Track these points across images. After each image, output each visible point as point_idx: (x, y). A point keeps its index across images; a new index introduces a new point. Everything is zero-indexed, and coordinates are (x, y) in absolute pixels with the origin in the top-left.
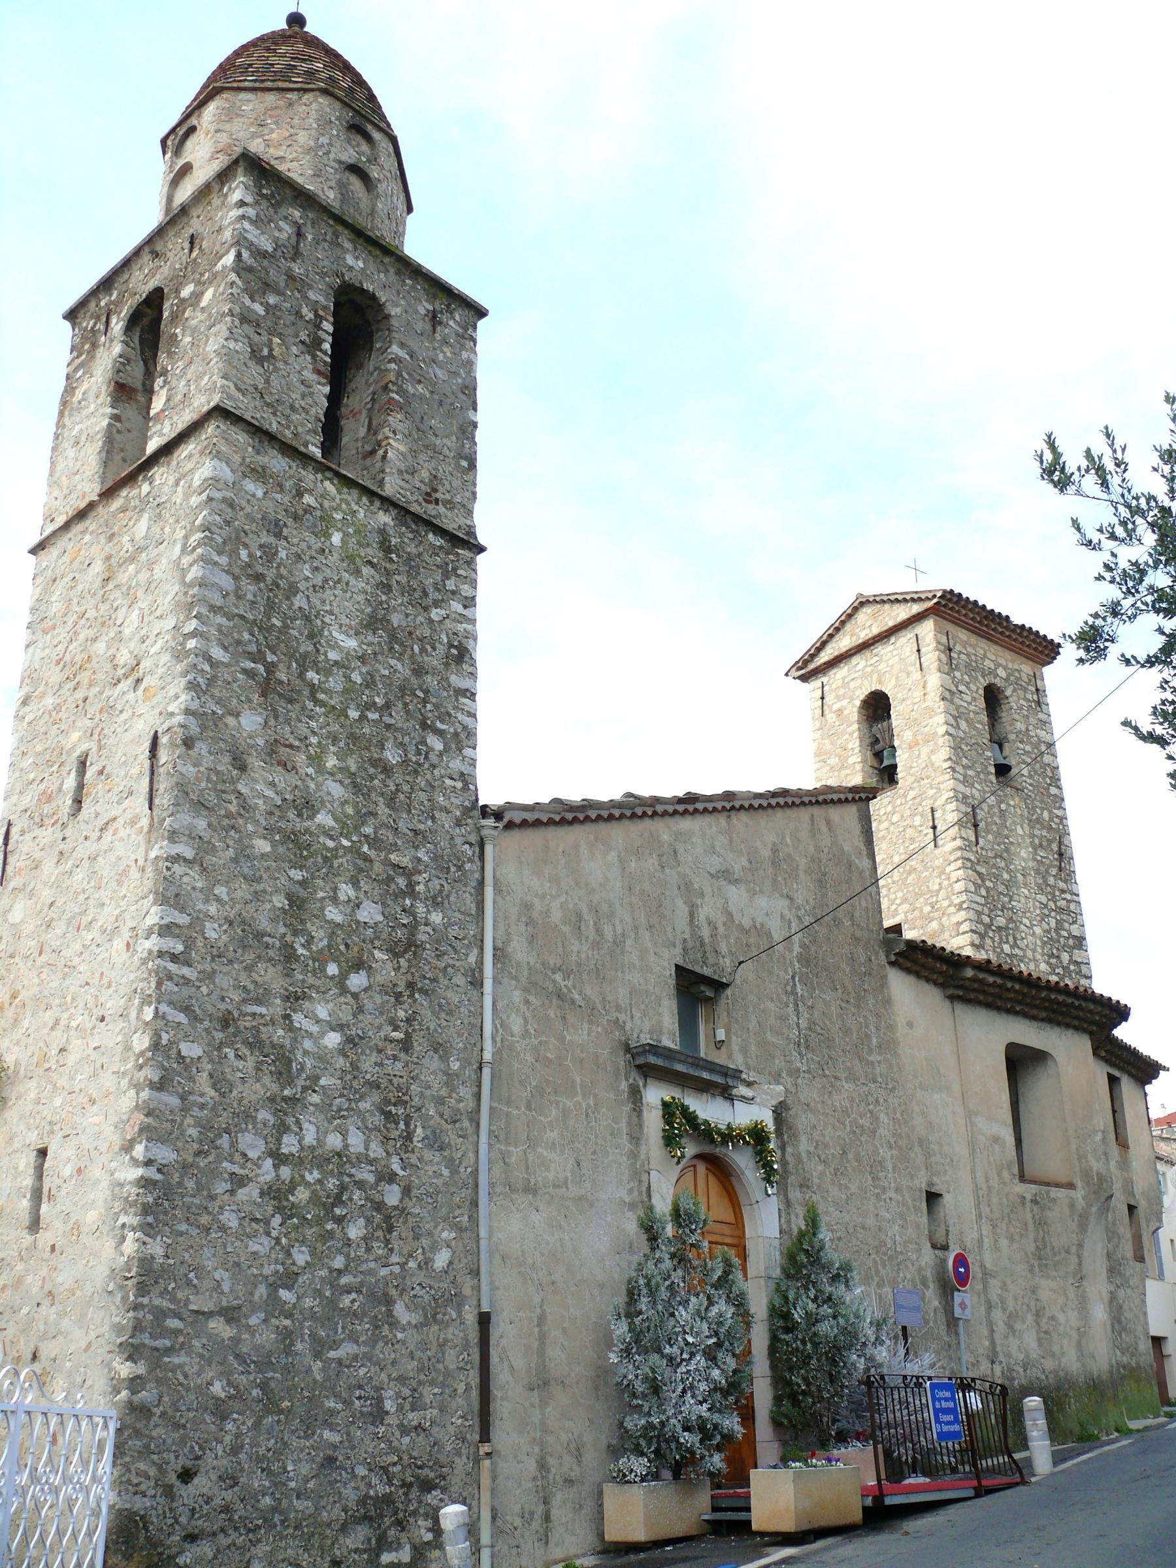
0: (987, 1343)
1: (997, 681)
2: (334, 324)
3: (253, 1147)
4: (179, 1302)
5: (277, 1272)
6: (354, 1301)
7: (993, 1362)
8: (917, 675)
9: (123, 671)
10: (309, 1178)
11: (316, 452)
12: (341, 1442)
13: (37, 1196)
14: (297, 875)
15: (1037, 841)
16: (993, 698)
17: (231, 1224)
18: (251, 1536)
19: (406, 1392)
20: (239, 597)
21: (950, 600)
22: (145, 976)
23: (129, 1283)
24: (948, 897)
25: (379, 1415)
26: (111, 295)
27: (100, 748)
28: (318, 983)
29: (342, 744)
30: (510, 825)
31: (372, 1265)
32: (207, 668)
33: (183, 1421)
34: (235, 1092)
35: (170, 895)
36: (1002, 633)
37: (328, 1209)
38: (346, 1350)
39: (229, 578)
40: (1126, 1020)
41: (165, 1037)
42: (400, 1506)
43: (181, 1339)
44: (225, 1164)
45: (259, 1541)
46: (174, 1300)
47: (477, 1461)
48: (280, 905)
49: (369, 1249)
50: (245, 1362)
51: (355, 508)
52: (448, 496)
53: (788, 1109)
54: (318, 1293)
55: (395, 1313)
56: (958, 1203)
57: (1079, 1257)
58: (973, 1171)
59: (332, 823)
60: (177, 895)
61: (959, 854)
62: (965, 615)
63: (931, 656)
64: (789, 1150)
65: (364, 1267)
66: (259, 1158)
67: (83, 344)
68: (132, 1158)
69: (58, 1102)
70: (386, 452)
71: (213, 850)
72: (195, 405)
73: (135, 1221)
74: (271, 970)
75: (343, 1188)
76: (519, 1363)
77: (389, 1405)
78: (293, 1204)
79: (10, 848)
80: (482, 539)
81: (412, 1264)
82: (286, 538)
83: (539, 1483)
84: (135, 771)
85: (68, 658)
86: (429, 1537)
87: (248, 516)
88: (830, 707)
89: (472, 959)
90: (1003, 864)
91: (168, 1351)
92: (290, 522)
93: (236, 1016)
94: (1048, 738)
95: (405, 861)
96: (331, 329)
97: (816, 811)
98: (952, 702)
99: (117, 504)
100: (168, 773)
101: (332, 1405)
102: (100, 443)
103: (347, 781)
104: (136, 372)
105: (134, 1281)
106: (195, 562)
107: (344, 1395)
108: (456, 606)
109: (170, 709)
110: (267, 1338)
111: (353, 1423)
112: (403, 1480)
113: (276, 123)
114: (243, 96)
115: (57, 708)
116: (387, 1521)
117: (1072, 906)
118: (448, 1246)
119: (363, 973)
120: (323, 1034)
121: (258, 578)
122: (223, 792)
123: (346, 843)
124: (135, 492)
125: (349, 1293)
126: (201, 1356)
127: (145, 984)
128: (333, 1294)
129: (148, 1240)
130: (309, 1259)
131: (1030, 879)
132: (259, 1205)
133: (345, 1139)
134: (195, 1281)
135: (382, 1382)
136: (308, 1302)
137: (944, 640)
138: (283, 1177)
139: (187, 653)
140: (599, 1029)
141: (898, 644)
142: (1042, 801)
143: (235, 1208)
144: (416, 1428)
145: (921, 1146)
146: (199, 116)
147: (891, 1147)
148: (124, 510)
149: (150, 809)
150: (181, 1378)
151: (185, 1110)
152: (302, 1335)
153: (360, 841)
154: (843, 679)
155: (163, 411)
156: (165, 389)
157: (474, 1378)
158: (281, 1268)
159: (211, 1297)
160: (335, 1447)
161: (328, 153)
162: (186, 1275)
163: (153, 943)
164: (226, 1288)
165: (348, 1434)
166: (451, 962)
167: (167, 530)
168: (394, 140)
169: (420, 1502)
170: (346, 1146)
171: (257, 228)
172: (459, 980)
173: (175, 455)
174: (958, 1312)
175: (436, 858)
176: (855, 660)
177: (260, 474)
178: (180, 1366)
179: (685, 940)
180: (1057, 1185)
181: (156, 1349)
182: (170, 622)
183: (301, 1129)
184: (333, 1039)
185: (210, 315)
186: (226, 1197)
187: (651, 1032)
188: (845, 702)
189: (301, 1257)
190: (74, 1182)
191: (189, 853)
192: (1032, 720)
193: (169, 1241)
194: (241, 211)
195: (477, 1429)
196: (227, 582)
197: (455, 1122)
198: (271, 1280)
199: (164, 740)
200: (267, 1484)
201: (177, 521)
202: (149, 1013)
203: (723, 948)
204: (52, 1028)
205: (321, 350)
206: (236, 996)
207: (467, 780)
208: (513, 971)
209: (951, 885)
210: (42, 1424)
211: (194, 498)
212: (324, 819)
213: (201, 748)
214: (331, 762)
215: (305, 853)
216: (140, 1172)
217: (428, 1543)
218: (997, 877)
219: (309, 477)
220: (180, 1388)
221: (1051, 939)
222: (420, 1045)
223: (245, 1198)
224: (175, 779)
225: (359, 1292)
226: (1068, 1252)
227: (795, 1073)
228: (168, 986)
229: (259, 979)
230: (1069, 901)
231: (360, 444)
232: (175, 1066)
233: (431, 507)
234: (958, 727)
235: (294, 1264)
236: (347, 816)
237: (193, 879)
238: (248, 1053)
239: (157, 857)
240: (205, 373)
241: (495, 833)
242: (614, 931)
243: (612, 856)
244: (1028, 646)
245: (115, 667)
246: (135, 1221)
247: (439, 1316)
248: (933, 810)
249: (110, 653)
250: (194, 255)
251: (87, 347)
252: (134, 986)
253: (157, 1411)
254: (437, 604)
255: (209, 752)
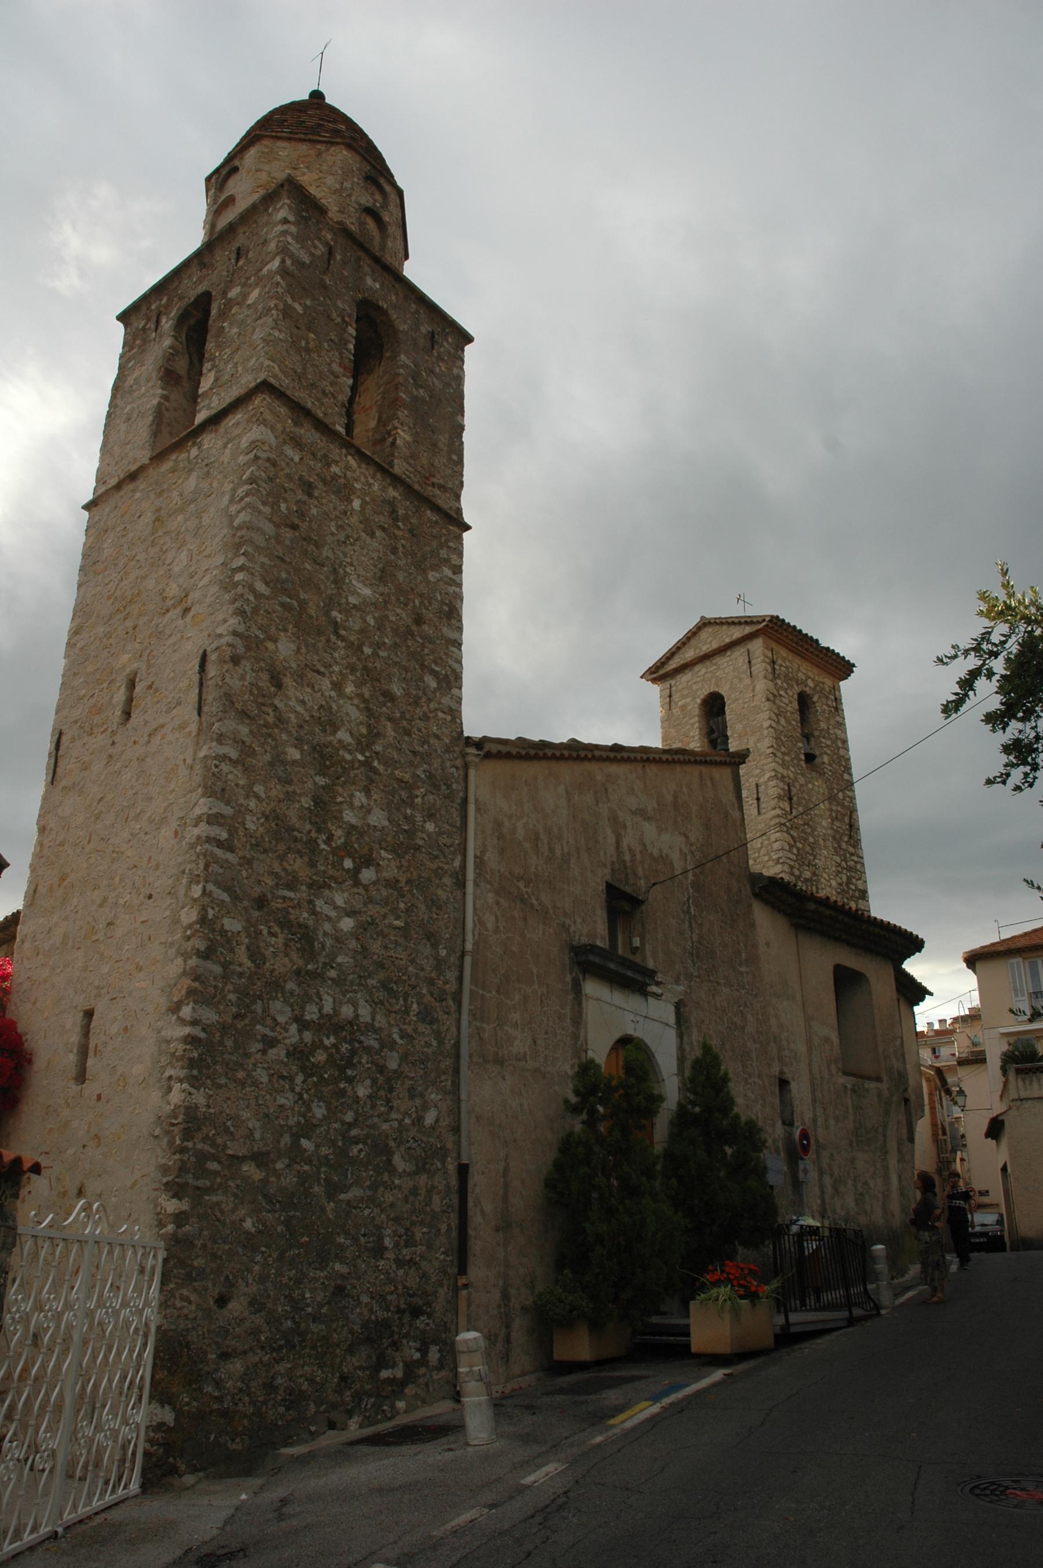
0: (819, 1201)
1: (807, 689)
2: (357, 330)
3: (282, 1013)
4: (218, 1146)
5: (299, 1123)
6: (360, 1151)
7: (823, 1217)
8: (748, 681)
9: (172, 602)
10: (327, 1042)
11: (340, 429)
12: (349, 1273)
13: (84, 1052)
14: (321, 781)
15: (834, 814)
16: (804, 702)
17: (262, 1080)
18: (275, 1354)
19: (402, 1231)
20: (279, 542)
21: (776, 624)
22: (193, 858)
23: (176, 1129)
24: (768, 854)
25: (379, 1251)
26: (161, 300)
27: (149, 667)
28: (337, 874)
29: (358, 674)
30: (488, 756)
31: (376, 1120)
32: (252, 598)
33: (219, 1253)
34: (268, 964)
35: (215, 788)
36: (812, 653)
37: (342, 1070)
38: (355, 1193)
39: (271, 525)
40: (920, 951)
41: (211, 913)
42: (396, 1329)
43: (219, 1180)
44: (258, 1027)
45: (282, 1359)
46: (214, 1144)
47: (456, 1290)
48: (307, 806)
49: (373, 1107)
50: (272, 1202)
51: (371, 481)
52: (441, 482)
53: (685, 1006)
54: (333, 1143)
55: (393, 1162)
56: (800, 1090)
57: (884, 1135)
58: (810, 1064)
59: (349, 740)
60: (223, 790)
61: (777, 820)
62: (786, 637)
63: (760, 666)
64: (685, 1039)
65: (369, 1122)
66: (286, 1023)
67: (134, 340)
68: (179, 1018)
69: (105, 969)
70: (395, 440)
71: (253, 753)
72: (243, 382)
73: (183, 1073)
74: (299, 861)
75: (353, 1052)
76: (488, 1207)
77: (387, 1242)
78: (313, 1064)
79: (61, 753)
80: (467, 518)
81: (407, 1121)
82: (317, 498)
83: (502, 1310)
84: (184, 684)
85: (118, 593)
86: (417, 1356)
87: (287, 475)
88: (676, 703)
89: (457, 864)
90: (809, 831)
91: (208, 1190)
92: (320, 485)
93: (270, 897)
94: (842, 736)
95: (407, 777)
96: (354, 333)
97: (704, 769)
98: (774, 702)
99: (167, 466)
100: (217, 685)
101: (342, 1240)
102: (151, 418)
103: (362, 706)
104: (181, 365)
105: (182, 1126)
106: (243, 509)
107: (353, 1232)
108: (448, 572)
109: (219, 631)
110: (289, 1181)
111: (359, 1257)
112: (398, 1307)
113: (307, 167)
114: (280, 144)
115: (108, 635)
116: (386, 1342)
117: (859, 866)
118: (436, 1106)
119: (372, 868)
120: (339, 918)
121: (294, 527)
122: (263, 705)
123: (360, 757)
124: (184, 456)
125: (357, 1143)
126: (236, 1195)
127: (194, 865)
128: (344, 1144)
129: (192, 1090)
130: (325, 1112)
131: (829, 843)
132: (286, 1065)
133: (356, 1010)
134: (232, 1129)
135: (382, 1222)
136: (324, 1151)
137: (769, 654)
138: (306, 1041)
139: (236, 585)
140: (551, 931)
141: (733, 656)
142: (838, 784)
143: (265, 1065)
144: (409, 1261)
145: (775, 1041)
146: (242, 158)
147: (755, 1042)
148: (174, 470)
149: (199, 715)
150: (218, 1214)
151: (225, 977)
152: (319, 1179)
153: (371, 757)
154: (688, 682)
155: (211, 389)
156: (213, 372)
157: (454, 1218)
158: (302, 1120)
159: (245, 1143)
160: (343, 1277)
161: (349, 196)
162: (224, 1124)
163: (203, 829)
164: (257, 1135)
165: (355, 1266)
166: (441, 864)
167: (215, 484)
168: (400, 193)
169: (411, 1326)
170: (357, 1016)
171: (297, 242)
172: (447, 881)
173: (223, 424)
174: (801, 1176)
175: (431, 776)
176: (697, 668)
177: (297, 443)
178: (218, 1204)
179: (613, 863)
180: (870, 1078)
181: (198, 1188)
182: (219, 560)
183: (321, 1000)
184: (347, 924)
185: (256, 310)
186: (258, 1056)
187: (588, 936)
188: (688, 700)
189: (319, 1111)
190: (120, 1039)
191: (234, 755)
192: (832, 722)
193: (211, 1093)
194: (285, 227)
195: (456, 1263)
196: (269, 528)
197: (442, 1000)
198: (294, 1130)
199: (213, 657)
200: (288, 1309)
201: (225, 477)
202: (197, 891)
203: (640, 872)
204: (101, 906)
205: (346, 349)
206: (270, 881)
207: (455, 714)
208: (488, 876)
209: (771, 844)
210: (108, 1253)
211: (241, 458)
212: (343, 735)
213: (246, 665)
214: (350, 689)
215: (328, 763)
216: (187, 1030)
217: (416, 1361)
218: (805, 840)
219: (335, 452)
220: (217, 1223)
221: (843, 890)
222: (417, 933)
223: (274, 1057)
224: (223, 690)
225: (365, 1143)
226: (876, 1131)
227: (689, 977)
228: (215, 868)
229: (288, 867)
230: (856, 862)
231: (370, 434)
232: (218, 938)
233: (430, 488)
234: (778, 722)
235: (313, 1117)
236: (362, 736)
237: (235, 776)
238: (279, 931)
239: (205, 757)
240: (251, 357)
241: (477, 760)
242: (562, 850)
243: (561, 789)
244: (831, 664)
245: (164, 599)
246: (183, 1073)
247: (427, 1166)
248: (757, 786)
249: (160, 587)
250: (240, 263)
251: (138, 342)
252: (182, 868)
253: (199, 1243)
254: (433, 568)
255: (252, 669)
